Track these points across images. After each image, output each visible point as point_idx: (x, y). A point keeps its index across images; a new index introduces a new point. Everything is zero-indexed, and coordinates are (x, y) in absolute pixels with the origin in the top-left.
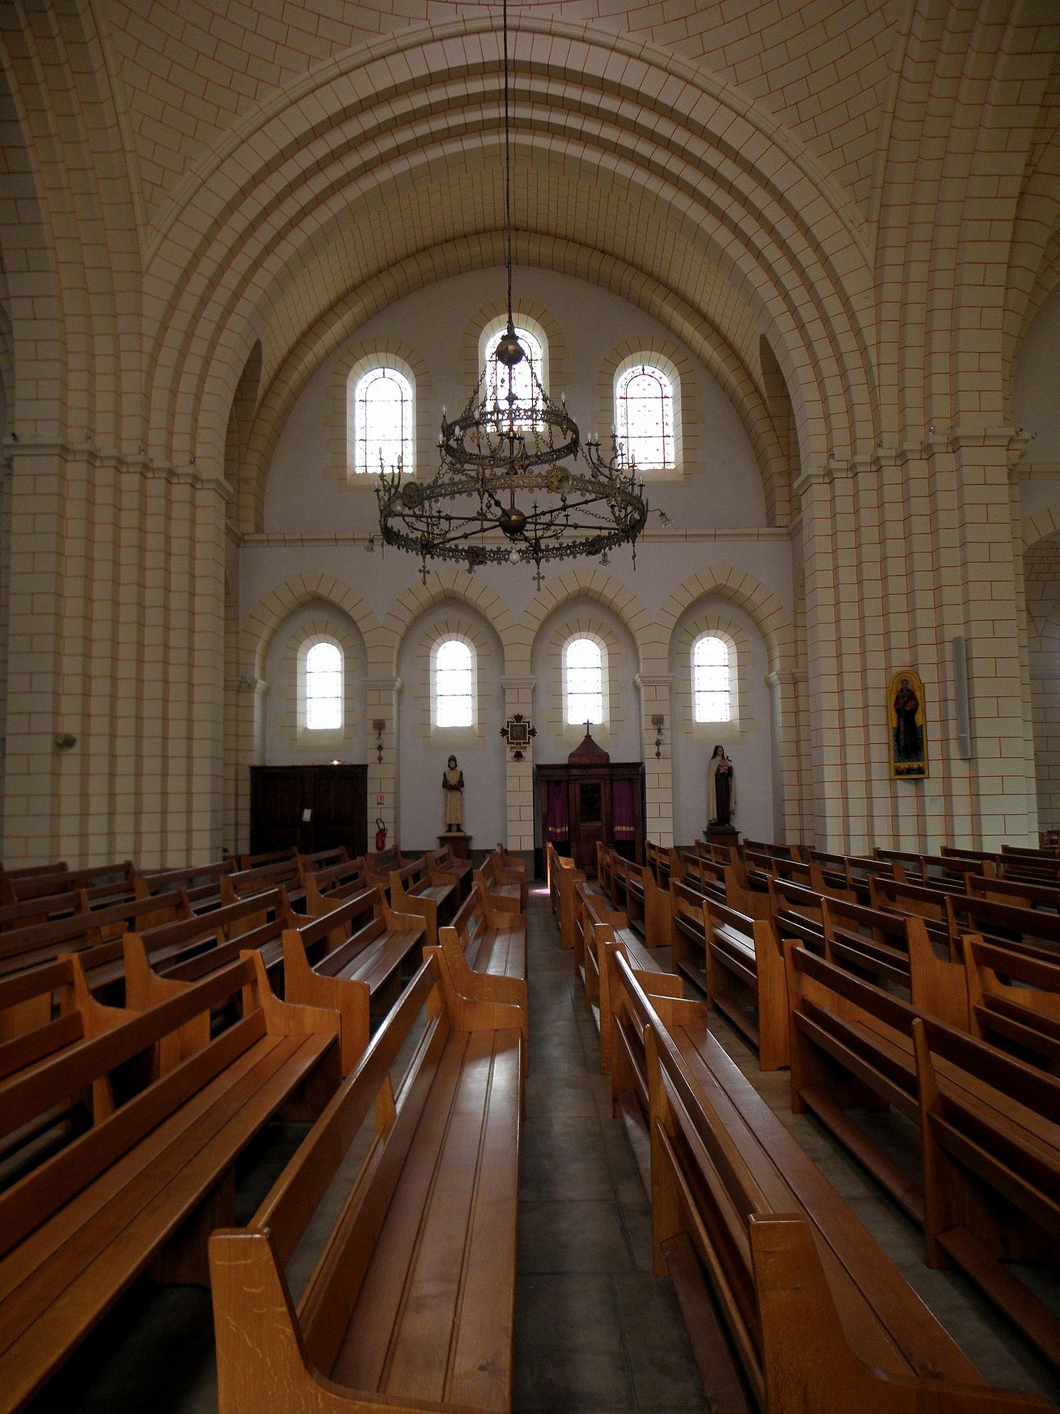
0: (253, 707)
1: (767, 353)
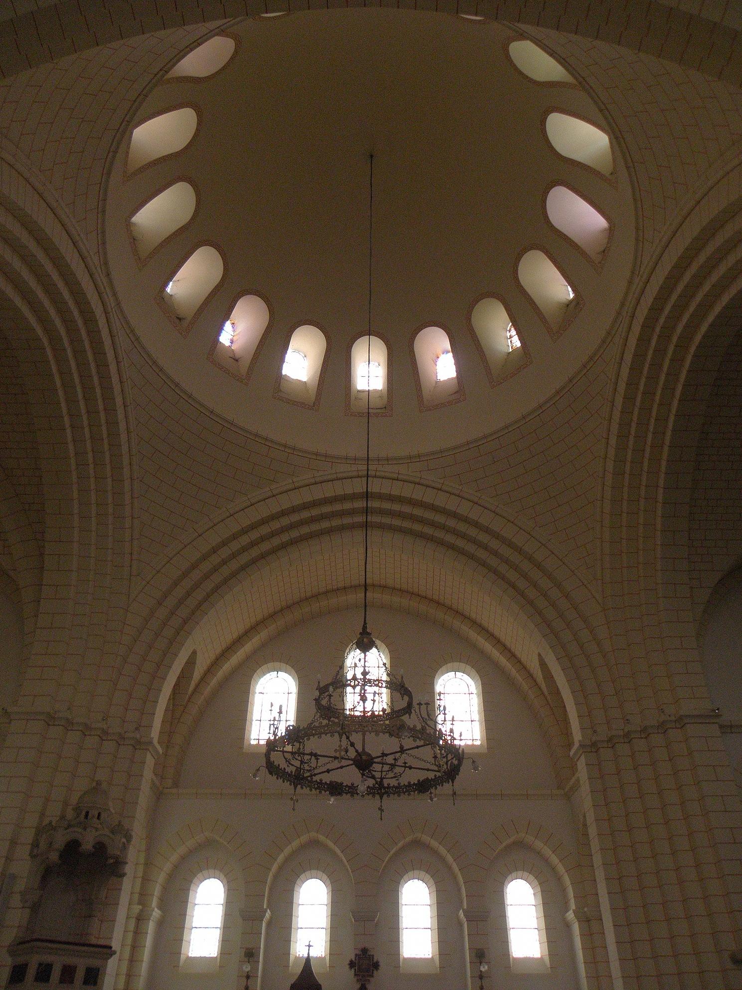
0: (147, 933)
1: (543, 664)
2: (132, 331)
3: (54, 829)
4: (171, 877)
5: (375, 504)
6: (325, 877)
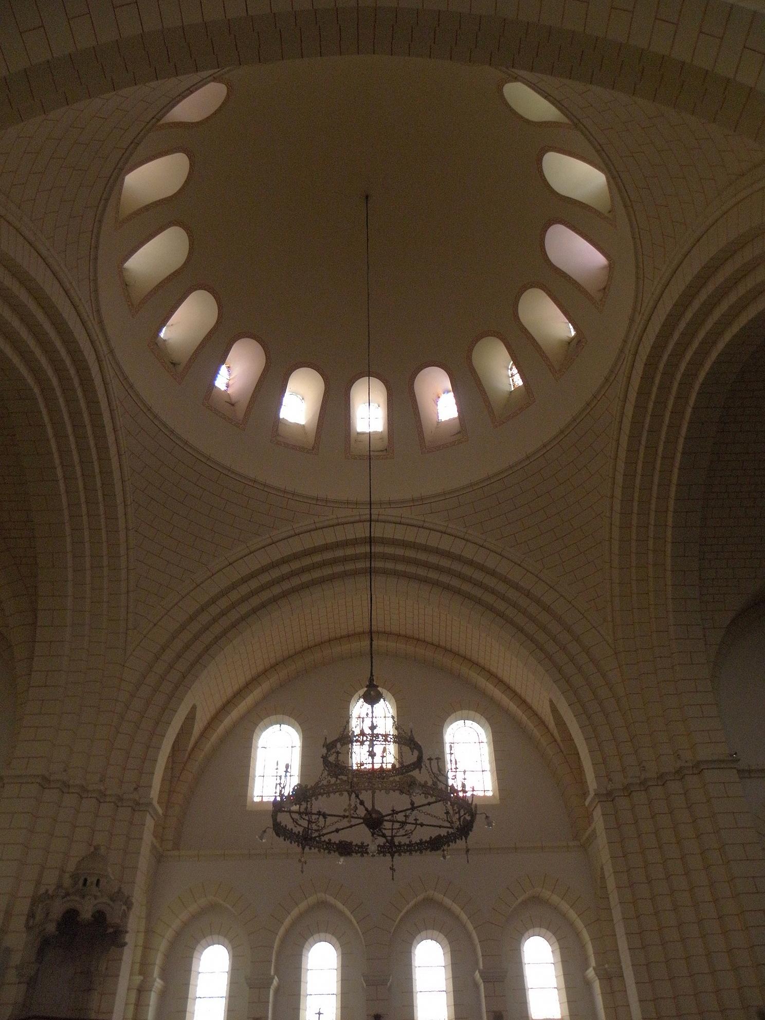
1: (554, 710)
2: (126, 378)
3: (52, 897)
4: (173, 944)
5: (377, 549)
6: (334, 940)
